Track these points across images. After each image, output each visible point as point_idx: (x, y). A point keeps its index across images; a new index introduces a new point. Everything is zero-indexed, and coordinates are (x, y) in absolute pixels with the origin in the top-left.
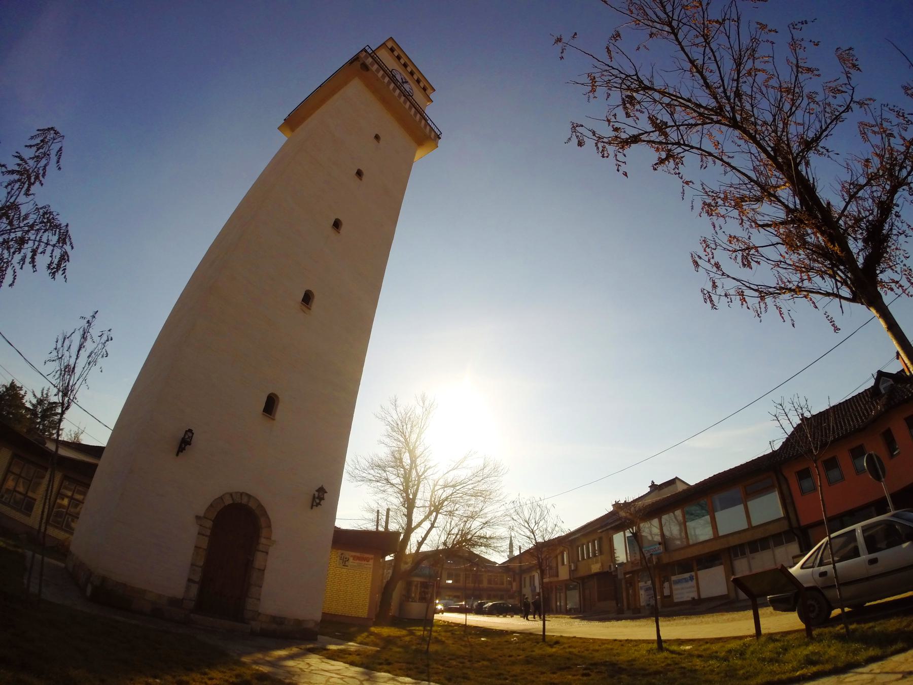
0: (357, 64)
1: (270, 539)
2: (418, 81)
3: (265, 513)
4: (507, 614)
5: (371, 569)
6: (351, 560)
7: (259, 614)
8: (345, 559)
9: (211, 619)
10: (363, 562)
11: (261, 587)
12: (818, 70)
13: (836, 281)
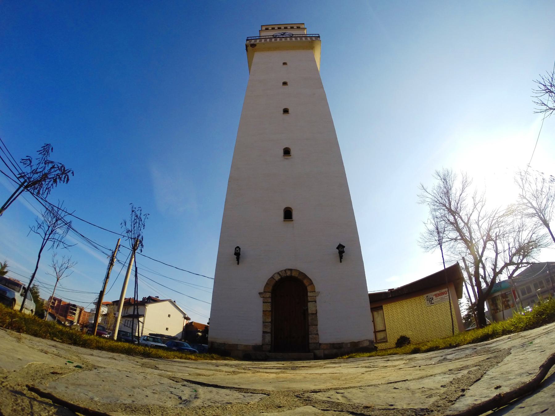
0: (249, 48)
1: (315, 292)
2: (292, 28)
3: (305, 276)
6: (434, 297)
7: (320, 344)
8: (430, 299)
9: (281, 354)
10: (443, 296)
11: (317, 325)
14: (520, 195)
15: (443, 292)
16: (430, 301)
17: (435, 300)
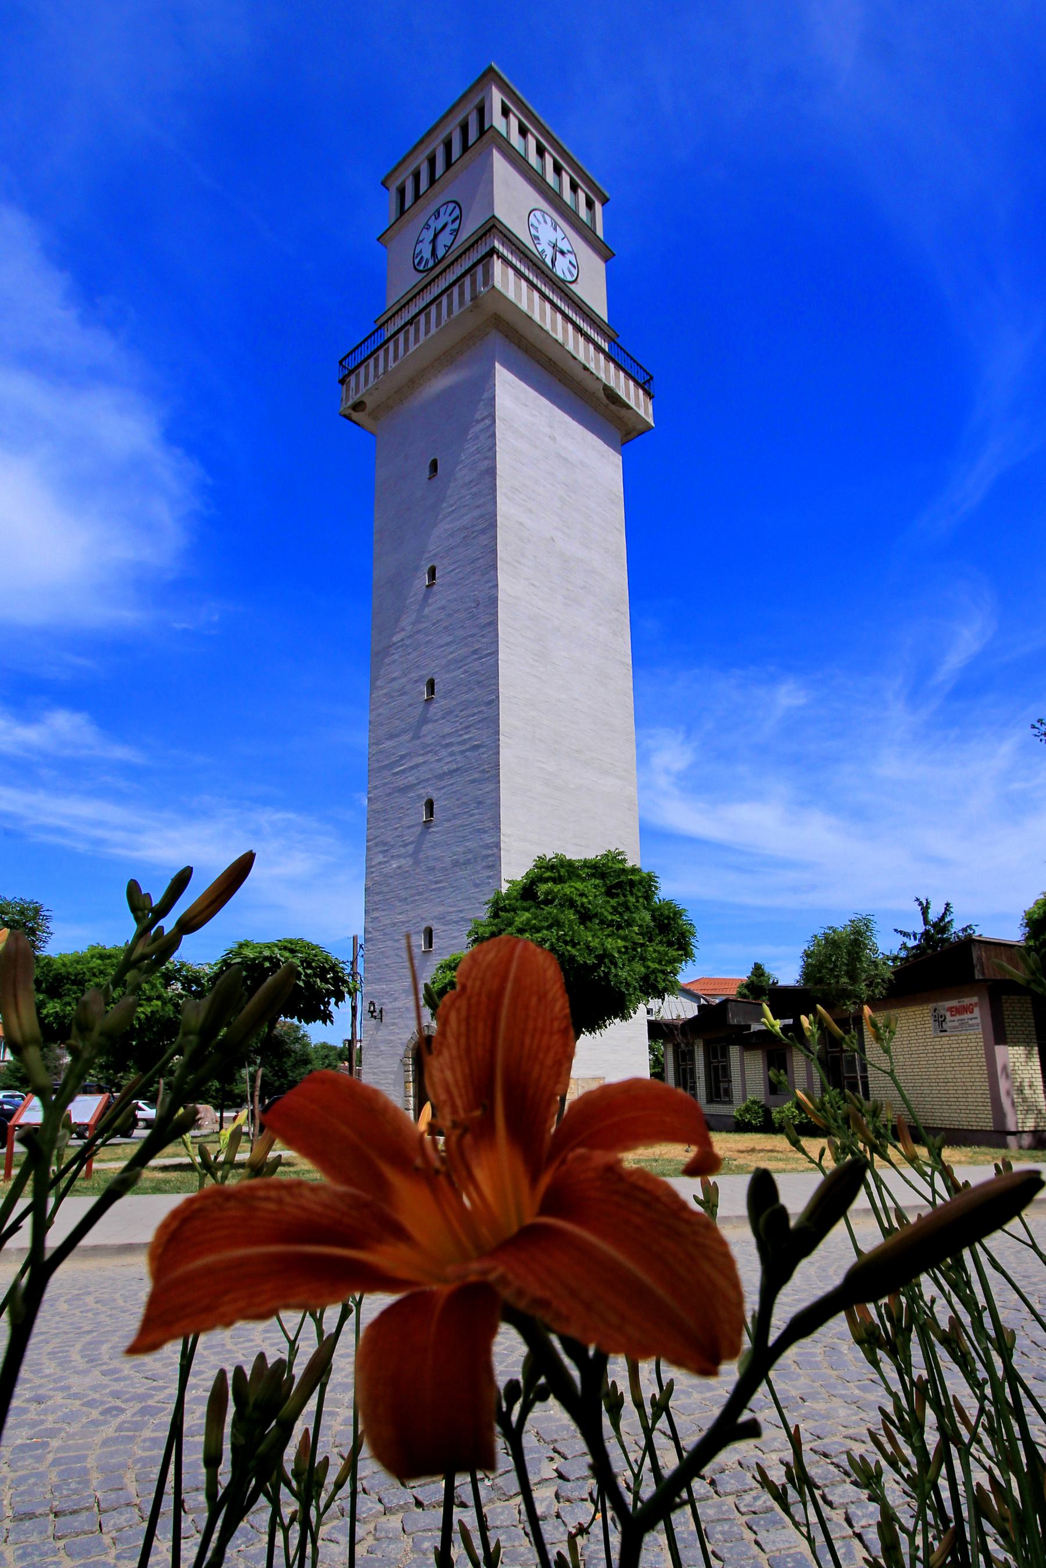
4: (1031, 929)
5: (980, 1027)
6: (948, 1014)
10: (966, 1016)
12: (355, 938)
13: (103, 1144)
14: (436, 218)
15: (965, 1004)
16: (940, 1020)
17: (950, 1024)
